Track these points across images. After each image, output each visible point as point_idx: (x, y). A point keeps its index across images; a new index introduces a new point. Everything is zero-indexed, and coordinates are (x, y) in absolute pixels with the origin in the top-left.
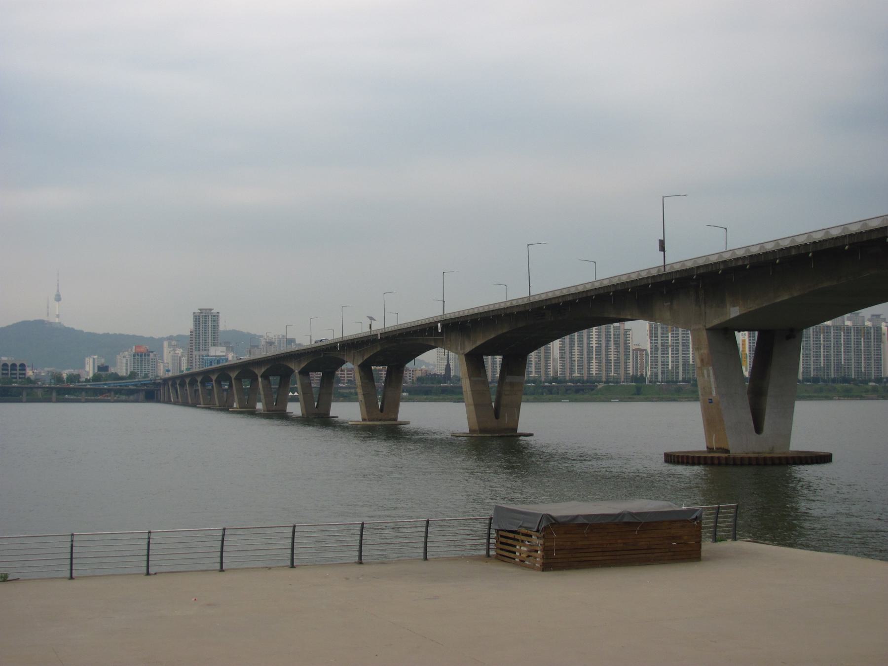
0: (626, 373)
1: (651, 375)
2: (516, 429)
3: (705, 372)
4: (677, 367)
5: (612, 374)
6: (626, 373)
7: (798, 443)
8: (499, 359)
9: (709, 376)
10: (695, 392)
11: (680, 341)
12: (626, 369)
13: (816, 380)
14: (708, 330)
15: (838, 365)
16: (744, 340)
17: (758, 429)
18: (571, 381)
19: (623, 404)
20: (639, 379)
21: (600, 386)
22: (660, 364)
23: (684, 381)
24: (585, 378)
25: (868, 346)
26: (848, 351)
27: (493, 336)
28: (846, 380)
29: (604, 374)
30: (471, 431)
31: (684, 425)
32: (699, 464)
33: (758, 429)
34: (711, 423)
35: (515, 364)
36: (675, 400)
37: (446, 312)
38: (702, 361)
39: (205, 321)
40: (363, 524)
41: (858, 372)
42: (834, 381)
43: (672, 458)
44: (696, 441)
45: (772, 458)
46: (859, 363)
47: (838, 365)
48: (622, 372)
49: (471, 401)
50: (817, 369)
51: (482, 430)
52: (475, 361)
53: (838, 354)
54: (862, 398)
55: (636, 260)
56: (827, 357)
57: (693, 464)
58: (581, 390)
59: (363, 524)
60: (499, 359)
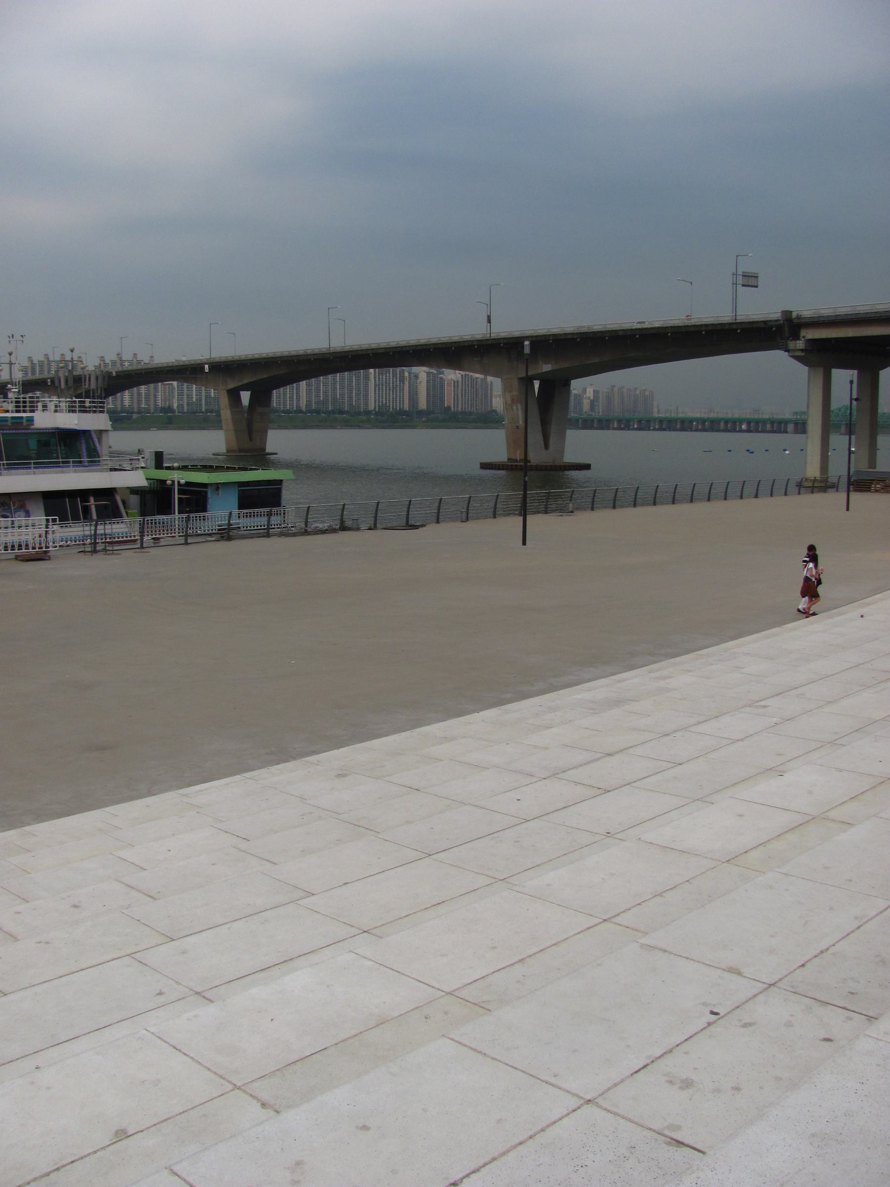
0: (156, 405)
1: (178, 407)
2: (265, 449)
3: (515, 408)
4: (201, 400)
5: (143, 406)
6: (156, 405)
7: (569, 457)
8: (249, 393)
9: (517, 410)
10: (220, 421)
11: (407, 383)
12: (155, 401)
13: (318, 412)
14: (520, 379)
15: (335, 400)
16: (537, 384)
17: (546, 447)
18: (284, 412)
19: (161, 432)
20: (168, 409)
21: (135, 416)
22: (185, 396)
23: (207, 411)
24: (119, 409)
25: (358, 384)
26: (342, 388)
27: (265, 376)
28: (341, 412)
29: (135, 406)
30: (228, 451)
31: (494, 445)
32: (503, 469)
33: (546, 447)
34: (511, 443)
35: (261, 395)
36: (204, 429)
37: (213, 356)
38: (513, 400)
39: (102, 358)
40: (344, 505)
41: (350, 405)
42: (333, 412)
43: (485, 466)
44: (501, 455)
45: (555, 466)
46: (350, 397)
47: (335, 400)
48: (152, 403)
49: (231, 426)
50: (317, 403)
51: (240, 451)
52: (234, 395)
53: (335, 389)
54: (360, 427)
55: (472, 329)
56: (325, 392)
57: (499, 469)
58: (637, 420)
59: (344, 505)
60: (249, 393)
